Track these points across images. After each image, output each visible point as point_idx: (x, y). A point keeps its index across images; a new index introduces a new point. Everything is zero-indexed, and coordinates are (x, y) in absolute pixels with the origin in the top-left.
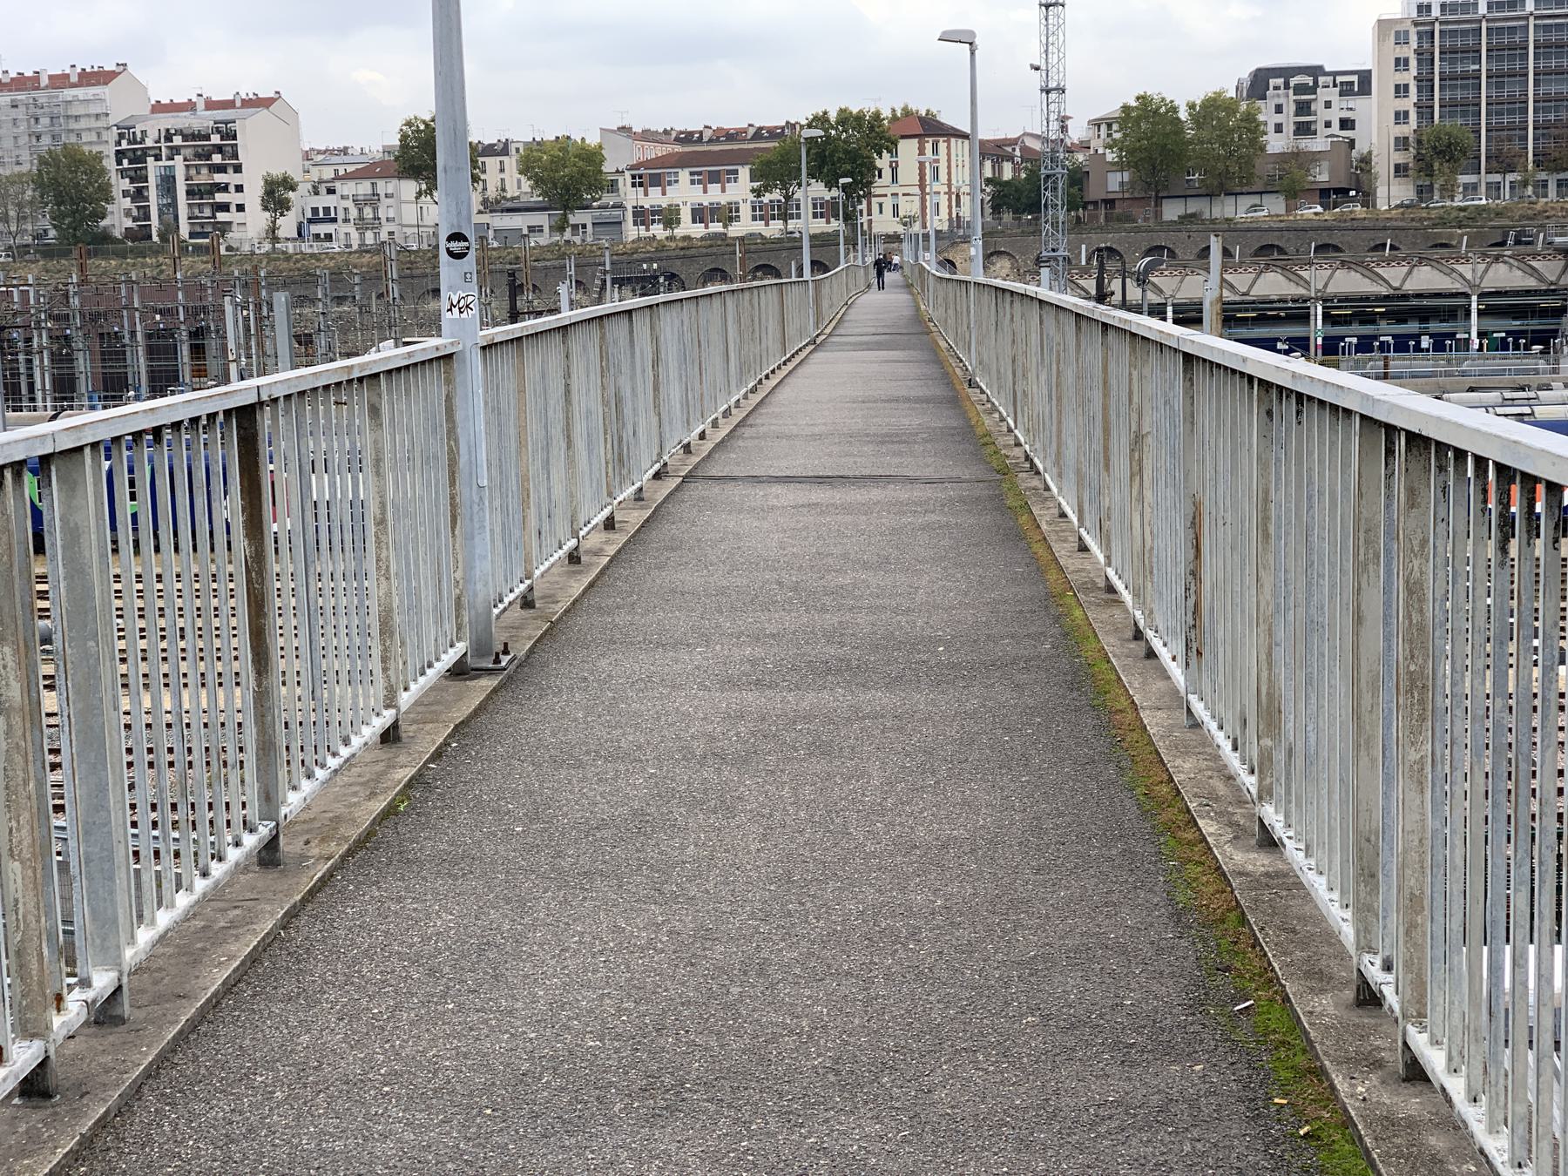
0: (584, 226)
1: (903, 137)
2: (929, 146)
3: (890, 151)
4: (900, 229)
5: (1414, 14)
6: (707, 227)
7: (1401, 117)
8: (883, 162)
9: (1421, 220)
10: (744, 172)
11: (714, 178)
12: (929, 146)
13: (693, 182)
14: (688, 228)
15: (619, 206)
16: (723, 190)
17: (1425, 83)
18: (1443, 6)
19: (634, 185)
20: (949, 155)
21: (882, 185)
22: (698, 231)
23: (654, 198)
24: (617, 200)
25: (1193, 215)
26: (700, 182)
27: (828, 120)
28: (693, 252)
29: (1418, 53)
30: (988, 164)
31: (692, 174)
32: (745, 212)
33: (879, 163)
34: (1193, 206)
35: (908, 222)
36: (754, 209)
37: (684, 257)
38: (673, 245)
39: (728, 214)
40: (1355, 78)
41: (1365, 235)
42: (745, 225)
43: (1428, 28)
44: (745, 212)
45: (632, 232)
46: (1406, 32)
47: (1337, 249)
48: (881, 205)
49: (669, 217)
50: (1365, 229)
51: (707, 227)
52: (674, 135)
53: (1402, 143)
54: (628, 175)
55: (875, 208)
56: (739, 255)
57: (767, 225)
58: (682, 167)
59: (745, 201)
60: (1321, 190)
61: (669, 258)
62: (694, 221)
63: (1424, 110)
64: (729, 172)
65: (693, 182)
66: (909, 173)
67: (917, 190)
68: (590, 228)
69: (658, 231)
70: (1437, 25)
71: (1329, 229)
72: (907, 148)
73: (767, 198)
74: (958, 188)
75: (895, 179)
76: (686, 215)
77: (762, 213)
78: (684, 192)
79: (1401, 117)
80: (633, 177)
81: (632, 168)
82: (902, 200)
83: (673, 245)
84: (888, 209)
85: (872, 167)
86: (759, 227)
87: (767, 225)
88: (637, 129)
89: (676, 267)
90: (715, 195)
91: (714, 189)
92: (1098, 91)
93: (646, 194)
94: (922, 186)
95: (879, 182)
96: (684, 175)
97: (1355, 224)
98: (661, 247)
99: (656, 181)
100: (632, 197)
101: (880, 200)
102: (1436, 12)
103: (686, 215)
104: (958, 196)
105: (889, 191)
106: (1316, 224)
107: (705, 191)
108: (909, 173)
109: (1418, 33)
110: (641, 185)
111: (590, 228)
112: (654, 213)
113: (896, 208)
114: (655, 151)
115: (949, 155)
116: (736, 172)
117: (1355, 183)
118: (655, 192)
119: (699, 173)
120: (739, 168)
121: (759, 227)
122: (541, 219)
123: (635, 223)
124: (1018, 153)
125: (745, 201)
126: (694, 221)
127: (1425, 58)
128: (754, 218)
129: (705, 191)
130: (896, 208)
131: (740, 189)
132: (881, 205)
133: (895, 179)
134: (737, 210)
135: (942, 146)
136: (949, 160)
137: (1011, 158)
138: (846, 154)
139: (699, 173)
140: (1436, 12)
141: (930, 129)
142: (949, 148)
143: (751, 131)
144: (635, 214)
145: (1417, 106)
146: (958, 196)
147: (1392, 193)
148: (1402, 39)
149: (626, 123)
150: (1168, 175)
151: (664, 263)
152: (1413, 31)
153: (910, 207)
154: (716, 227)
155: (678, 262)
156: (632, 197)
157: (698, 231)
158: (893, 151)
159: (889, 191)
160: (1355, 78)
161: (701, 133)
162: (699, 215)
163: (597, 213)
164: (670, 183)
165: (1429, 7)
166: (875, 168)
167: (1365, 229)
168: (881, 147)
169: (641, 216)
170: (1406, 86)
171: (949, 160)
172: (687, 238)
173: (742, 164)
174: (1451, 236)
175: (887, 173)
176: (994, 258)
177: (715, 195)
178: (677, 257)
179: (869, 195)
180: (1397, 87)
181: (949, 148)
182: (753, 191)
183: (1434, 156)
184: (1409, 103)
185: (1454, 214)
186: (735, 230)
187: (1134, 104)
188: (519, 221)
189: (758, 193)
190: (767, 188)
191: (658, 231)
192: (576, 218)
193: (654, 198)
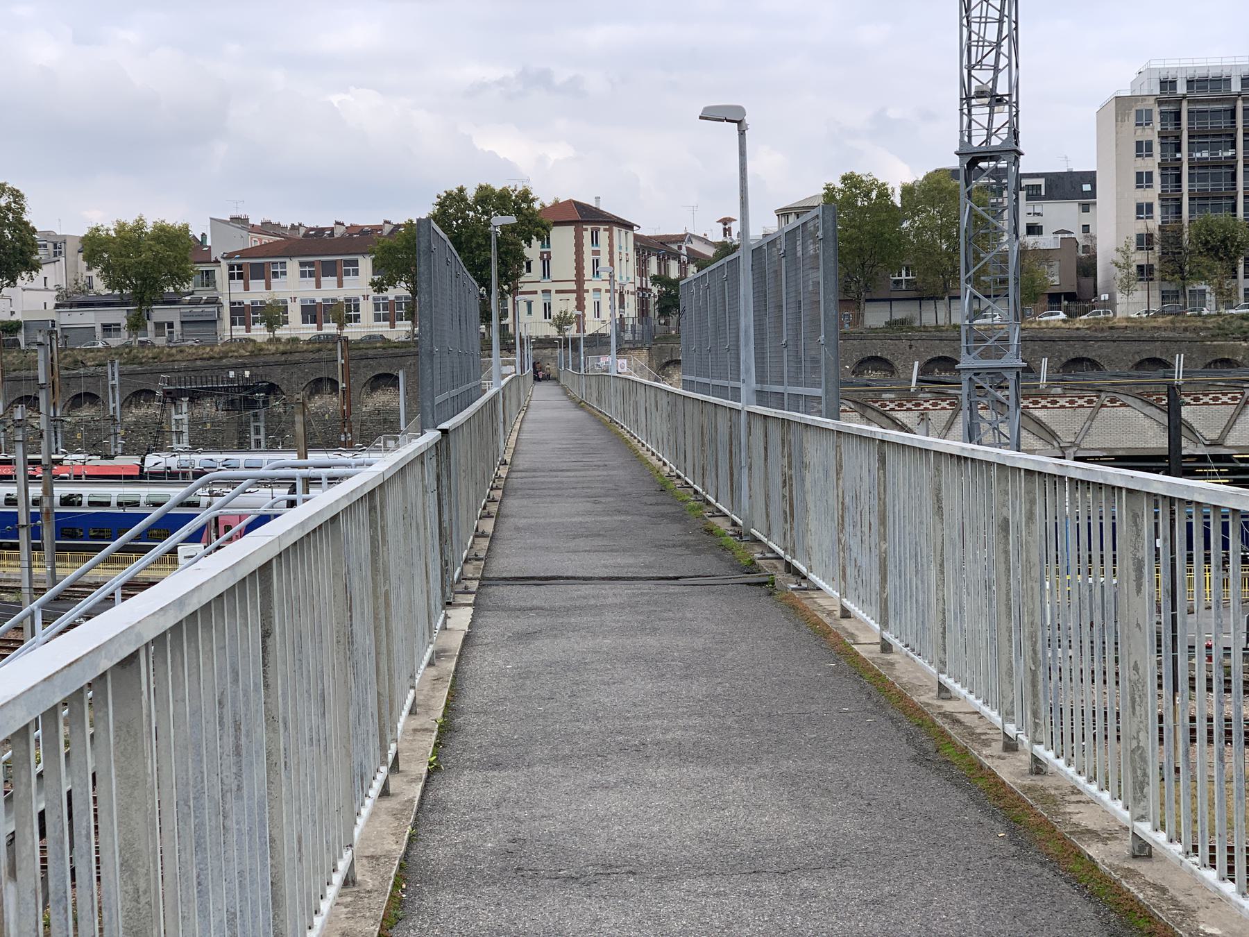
0: (171, 325)
1: (557, 224)
2: (587, 235)
3: (540, 237)
4: (553, 332)
5: (1157, 91)
6: (320, 328)
7: (1144, 210)
8: (532, 251)
9: (1195, 330)
10: (365, 264)
11: (329, 269)
12: (587, 235)
13: (303, 274)
14: (297, 328)
15: (214, 301)
16: (340, 285)
17: (1171, 172)
18: (1190, 82)
19: (232, 277)
20: (611, 245)
21: (531, 279)
22: (308, 331)
23: (257, 292)
24: (213, 294)
25: (903, 322)
26: (311, 274)
27: (464, 199)
28: (297, 357)
29: (1162, 136)
30: (653, 261)
31: (302, 264)
32: (367, 310)
33: (527, 252)
34: (901, 312)
35: (562, 322)
36: (377, 308)
37: (285, 363)
38: (272, 348)
39: (346, 312)
40: (1042, 182)
41: (1127, 347)
42: (364, 327)
43: (1172, 108)
44: (367, 310)
45: (229, 331)
46: (1149, 112)
47: (1094, 365)
48: (529, 304)
49: (273, 315)
50: (1127, 340)
51: (320, 328)
52: (302, 231)
53: (1145, 241)
54: (224, 264)
55: (523, 307)
56: (341, 361)
57: (393, 326)
58: (291, 256)
59: (366, 297)
60: (1050, 295)
61: (266, 364)
62: (304, 321)
63: (1171, 203)
64: (347, 263)
65: (303, 274)
66: (563, 266)
67: (573, 286)
68: (177, 326)
69: (259, 333)
70: (1185, 104)
71: (1083, 339)
72: (562, 238)
73: (391, 293)
74: (622, 286)
75: (546, 272)
76: (295, 313)
77: (387, 312)
78: (293, 286)
79: (1144, 210)
80: (231, 267)
81: (230, 256)
82: (555, 300)
83: (272, 348)
84: (538, 308)
85: (519, 257)
86: (382, 329)
87: (393, 326)
88: (255, 221)
89: (277, 376)
90: (330, 289)
91: (329, 283)
92: (790, 176)
93: (247, 288)
94: (580, 279)
95: (526, 277)
96: (293, 266)
97: (1116, 334)
98: (258, 350)
99: (259, 272)
100: (231, 291)
101: (529, 297)
102: (1182, 89)
103: (295, 313)
104: (621, 295)
105: (539, 288)
106: (1065, 333)
107: (318, 285)
108: (563, 266)
109: (1161, 113)
110: (240, 276)
111: (177, 326)
112: (255, 310)
113: (547, 307)
114: (253, 241)
115: (611, 245)
116: (355, 263)
117: (1079, 293)
118: (257, 286)
119: (311, 264)
120: (360, 258)
121: (382, 329)
122: (118, 316)
123: (233, 323)
124: (684, 251)
125: (366, 297)
126: (304, 321)
127: (1171, 143)
128: (377, 318)
129: (318, 285)
130: (547, 307)
131: (359, 283)
132: (529, 304)
133: (546, 272)
134: (357, 308)
135: (603, 236)
136: (611, 253)
137: (677, 256)
138: (486, 239)
139: (311, 264)
140: (1182, 89)
141: (585, 217)
142: (611, 238)
143: (388, 228)
144: (234, 311)
145: (1162, 198)
146: (621, 295)
147: (1133, 305)
148: (1143, 119)
149: (240, 213)
150: (895, 274)
151: (261, 371)
152: (1156, 110)
153: (564, 304)
154: (330, 328)
155: (279, 370)
156: (231, 291)
157: (308, 331)
158: (546, 241)
159: (539, 288)
160: (1042, 182)
161: (332, 229)
162: (311, 313)
163: (186, 309)
164: (275, 274)
165: (1173, 83)
166: (523, 257)
167: (1127, 340)
168: (530, 233)
169: (240, 313)
170: (1150, 174)
171: (611, 253)
172: (295, 340)
173: (363, 254)
174: (1235, 351)
175: (537, 266)
176: (670, 369)
177: (330, 289)
178: (278, 364)
179: (515, 291)
180: (1139, 175)
181: (611, 238)
182: (373, 284)
183: (1176, 259)
184: (1152, 195)
185: (1237, 323)
186: (353, 332)
187: (840, 186)
188: (90, 318)
189: (378, 286)
190: (392, 282)
191: (259, 333)
192: (161, 314)
193: (257, 292)
